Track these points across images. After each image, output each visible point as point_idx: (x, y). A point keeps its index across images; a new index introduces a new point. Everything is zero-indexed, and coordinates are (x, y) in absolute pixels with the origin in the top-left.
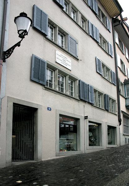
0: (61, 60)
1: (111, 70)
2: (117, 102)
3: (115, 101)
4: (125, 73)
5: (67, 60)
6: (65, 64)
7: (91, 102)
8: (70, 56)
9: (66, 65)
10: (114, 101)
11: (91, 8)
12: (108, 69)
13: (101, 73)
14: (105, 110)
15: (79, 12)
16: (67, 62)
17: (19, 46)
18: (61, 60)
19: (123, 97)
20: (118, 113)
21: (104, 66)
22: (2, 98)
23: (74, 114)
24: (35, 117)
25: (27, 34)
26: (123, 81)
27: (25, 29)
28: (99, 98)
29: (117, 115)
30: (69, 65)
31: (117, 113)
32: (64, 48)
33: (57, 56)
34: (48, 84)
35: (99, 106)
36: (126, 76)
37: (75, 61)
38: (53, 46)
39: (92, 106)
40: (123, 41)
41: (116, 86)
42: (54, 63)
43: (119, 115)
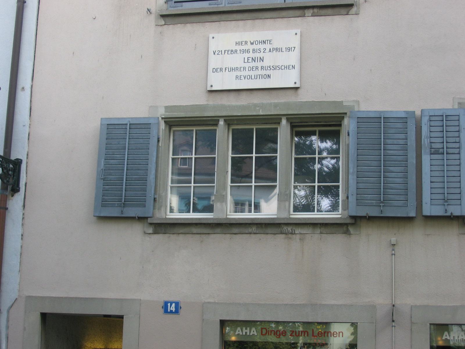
8: (298, 12)
38: (337, 18)
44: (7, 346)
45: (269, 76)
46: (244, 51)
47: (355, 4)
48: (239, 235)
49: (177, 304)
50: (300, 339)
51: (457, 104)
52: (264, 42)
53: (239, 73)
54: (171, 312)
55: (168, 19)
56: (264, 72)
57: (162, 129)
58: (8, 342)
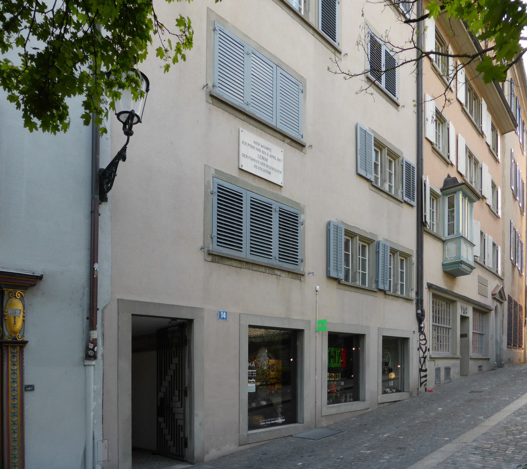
1: (401, 159)
2: (414, 259)
3: (410, 256)
5: (272, 156)
6: (266, 168)
7: (335, 276)
8: (282, 137)
9: (265, 171)
10: (406, 256)
12: (394, 156)
13: (368, 177)
14: (376, 292)
16: (271, 162)
17: (124, 159)
19: (436, 237)
20: (417, 294)
21: (379, 145)
22: (105, 307)
23: (289, 318)
25: (139, 121)
26: (441, 185)
27: (130, 110)
30: (278, 171)
31: (413, 295)
32: (303, 13)
33: (244, 149)
35: (364, 282)
36: (452, 165)
37: (294, 153)
38: (231, 117)
40: (482, 96)
41: (415, 209)
42: (235, 173)
44: (103, 342)
45: (270, 173)
47: (307, 149)
48: (257, 272)
51: (488, 297)
52: (268, 149)
54: (223, 318)
55: (215, 101)
57: (500, 320)
58: (103, 339)
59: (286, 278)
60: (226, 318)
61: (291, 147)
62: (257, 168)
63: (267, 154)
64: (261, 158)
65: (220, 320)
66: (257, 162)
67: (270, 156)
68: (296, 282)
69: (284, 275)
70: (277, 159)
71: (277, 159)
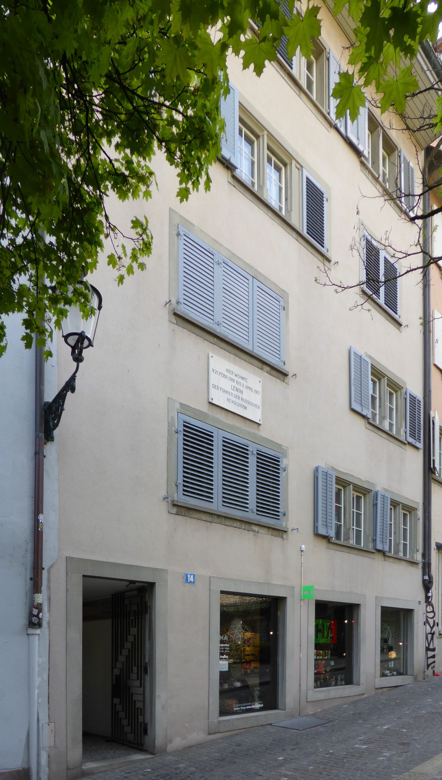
0: (225, 391)
1: (404, 390)
4: (329, 114)
6: (241, 402)
8: (260, 365)
9: (239, 405)
11: (342, 130)
15: (294, 162)
16: (246, 395)
18: (227, 392)
20: (424, 555)
22: (51, 567)
24: (150, 607)
28: (405, 524)
29: (416, 564)
30: (256, 406)
31: (419, 557)
33: (214, 379)
34: (409, 540)
35: (358, 541)
39: (331, 546)
41: (421, 452)
42: (205, 408)
43: (424, 564)
44: (50, 608)
46: (233, 380)
47: (290, 379)
49: (194, 576)
50: (65, 160)
53: (229, 397)
54: (191, 582)
55: (180, 320)
56: (243, 404)
58: (50, 603)
59: (265, 535)
60: (194, 582)
61: (271, 376)
62: (231, 401)
63: (242, 385)
64: (235, 389)
65: (187, 585)
66: (230, 394)
67: (246, 388)
68: (277, 540)
69: (263, 531)
70: (254, 391)
71: (254, 391)
